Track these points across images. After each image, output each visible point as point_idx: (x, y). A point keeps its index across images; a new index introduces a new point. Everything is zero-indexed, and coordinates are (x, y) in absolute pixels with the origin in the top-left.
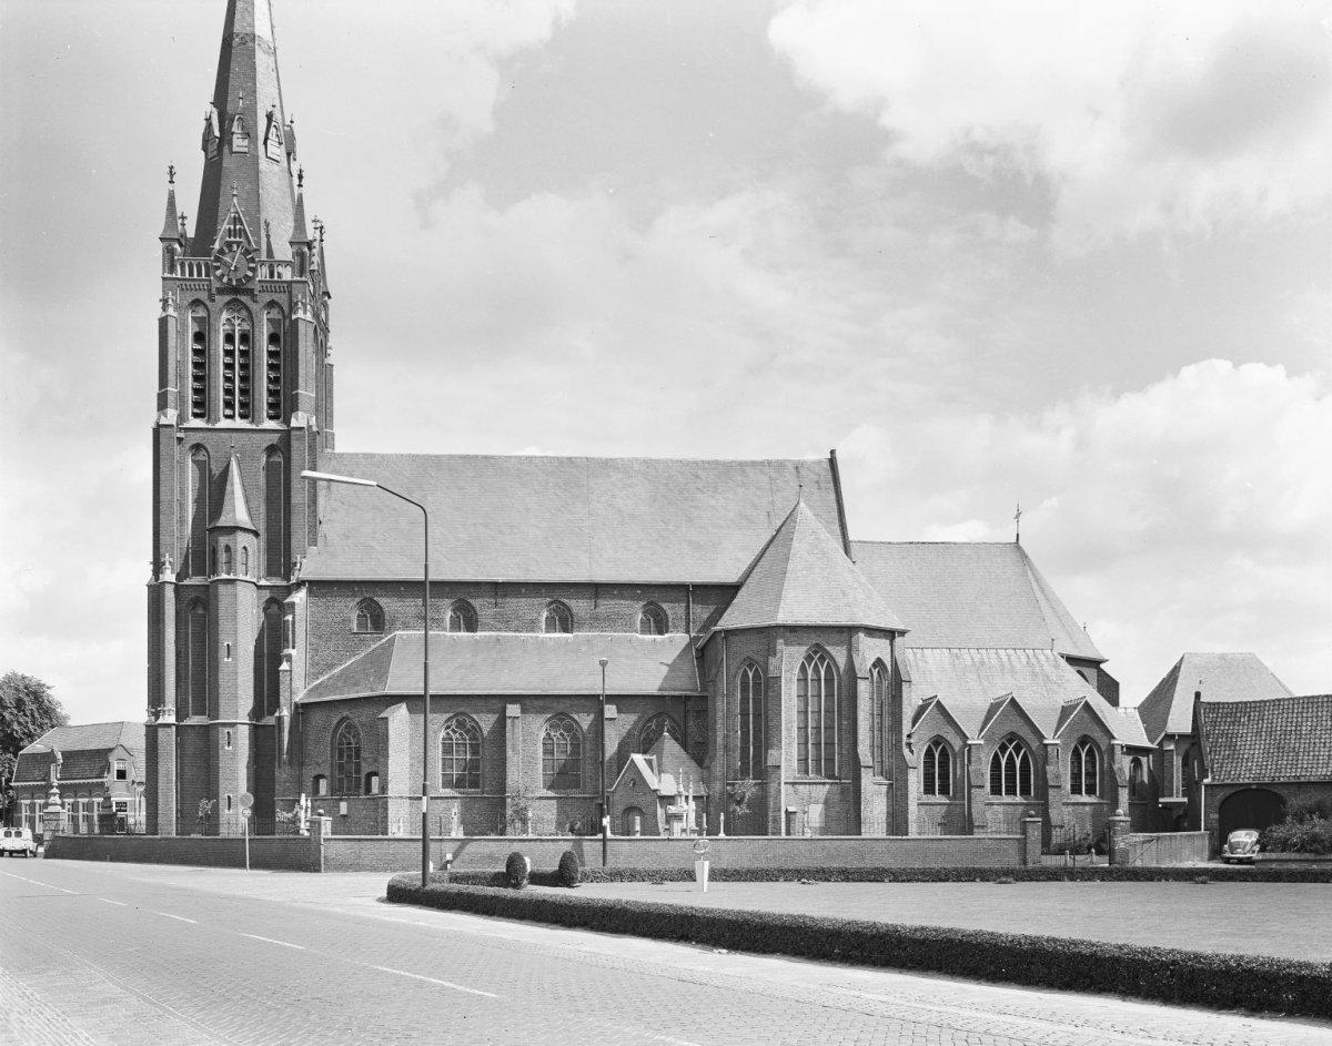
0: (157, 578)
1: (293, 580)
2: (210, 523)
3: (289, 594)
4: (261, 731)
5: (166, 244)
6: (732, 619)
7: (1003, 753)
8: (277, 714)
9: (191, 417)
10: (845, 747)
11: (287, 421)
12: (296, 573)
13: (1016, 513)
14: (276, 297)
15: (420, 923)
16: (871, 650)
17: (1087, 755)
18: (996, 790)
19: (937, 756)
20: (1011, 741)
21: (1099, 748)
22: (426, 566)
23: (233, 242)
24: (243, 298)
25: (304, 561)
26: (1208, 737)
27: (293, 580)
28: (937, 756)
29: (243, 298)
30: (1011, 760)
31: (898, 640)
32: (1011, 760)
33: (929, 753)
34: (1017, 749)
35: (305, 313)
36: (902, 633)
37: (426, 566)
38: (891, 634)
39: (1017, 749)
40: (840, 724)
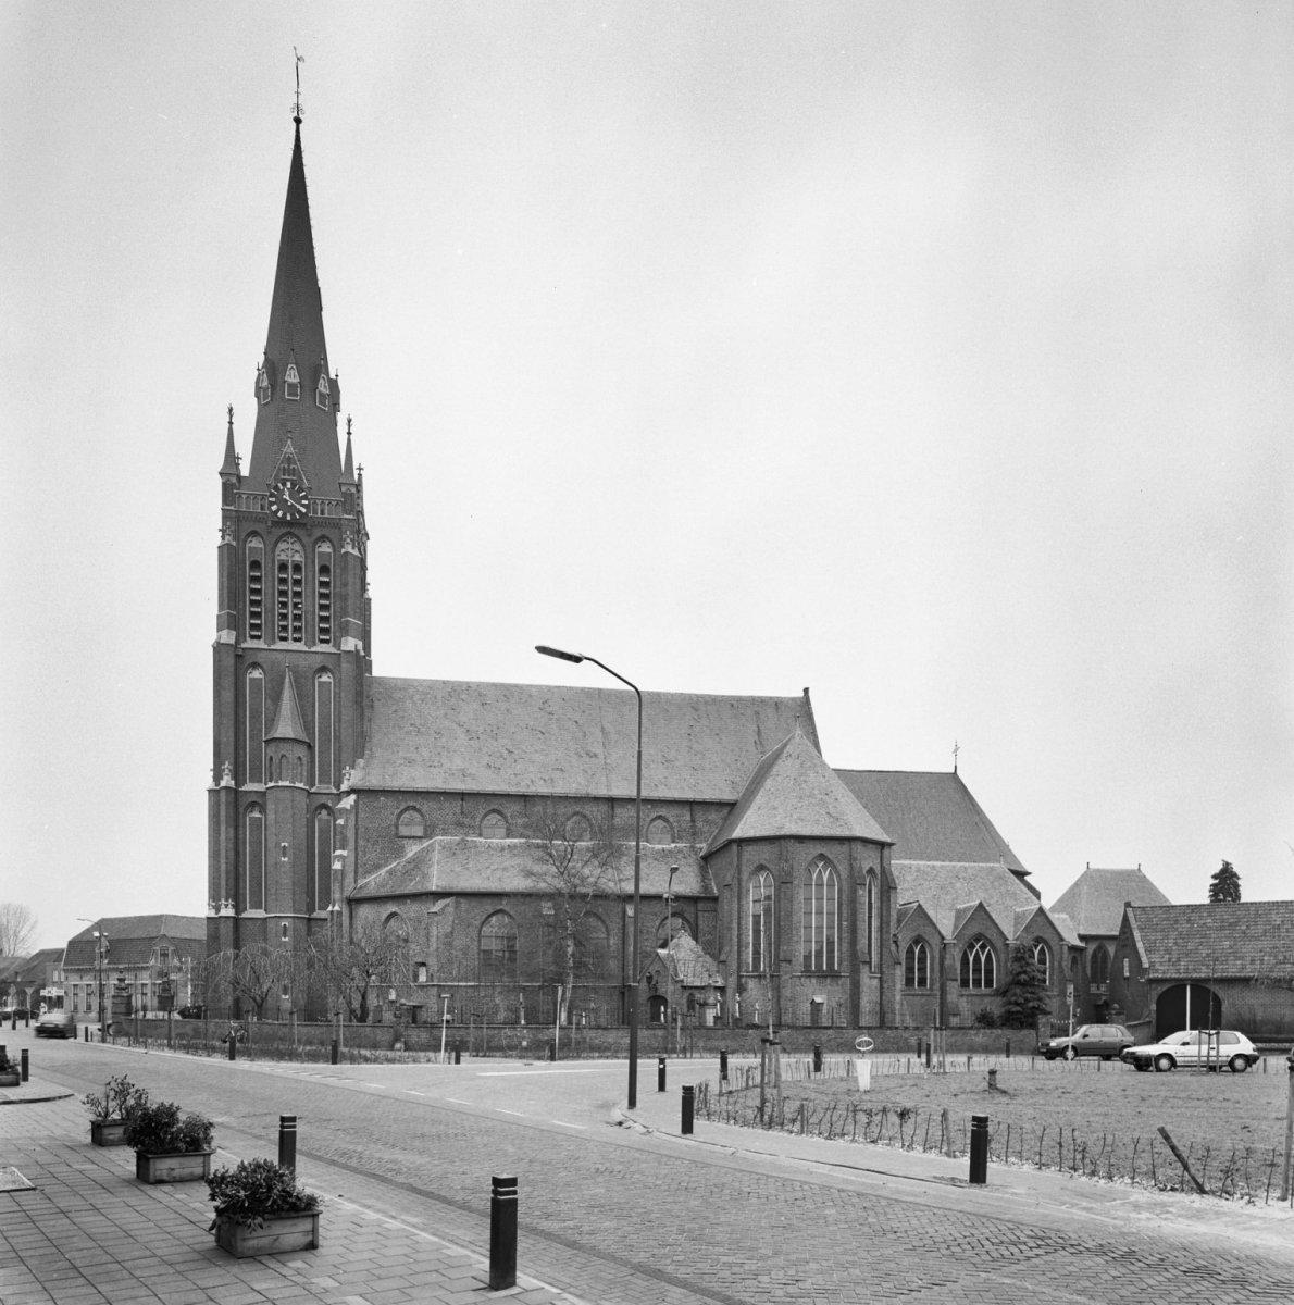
0: (217, 784)
1: (344, 787)
2: (266, 734)
3: (340, 800)
4: (313, 923)
5: (226, 478)
6: (746, 827)
7: (1036, 947)
8: (330, 908)
9: (248, 639)
10: (845, 945)
11: (337, 645)
12: (345, 782)
13: (954, 747)
14: (326, 532)
15: (413, 1092)
16: (868, 860)
17: (1039, 954)
18: (965, 983)
19: (917, 952)
20: (978, 940)
21: (1050, 948)
22: (640, 753)
23: (288, 480)
24: (296, 531)
25: (353, 772)
26: (325, 987)
27: (344, 787)
28: (917, 952)
29: (296, 531)
30: (977, 958)
31: (886, 852)
32: (977, 958)
33: (910, 951)
34: (983, 947)
35: (353, 548)
36: (891, 845)
37: (640, 753)
38: (882, 845)
39: (983, 947)
40: (840, 925)
